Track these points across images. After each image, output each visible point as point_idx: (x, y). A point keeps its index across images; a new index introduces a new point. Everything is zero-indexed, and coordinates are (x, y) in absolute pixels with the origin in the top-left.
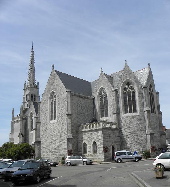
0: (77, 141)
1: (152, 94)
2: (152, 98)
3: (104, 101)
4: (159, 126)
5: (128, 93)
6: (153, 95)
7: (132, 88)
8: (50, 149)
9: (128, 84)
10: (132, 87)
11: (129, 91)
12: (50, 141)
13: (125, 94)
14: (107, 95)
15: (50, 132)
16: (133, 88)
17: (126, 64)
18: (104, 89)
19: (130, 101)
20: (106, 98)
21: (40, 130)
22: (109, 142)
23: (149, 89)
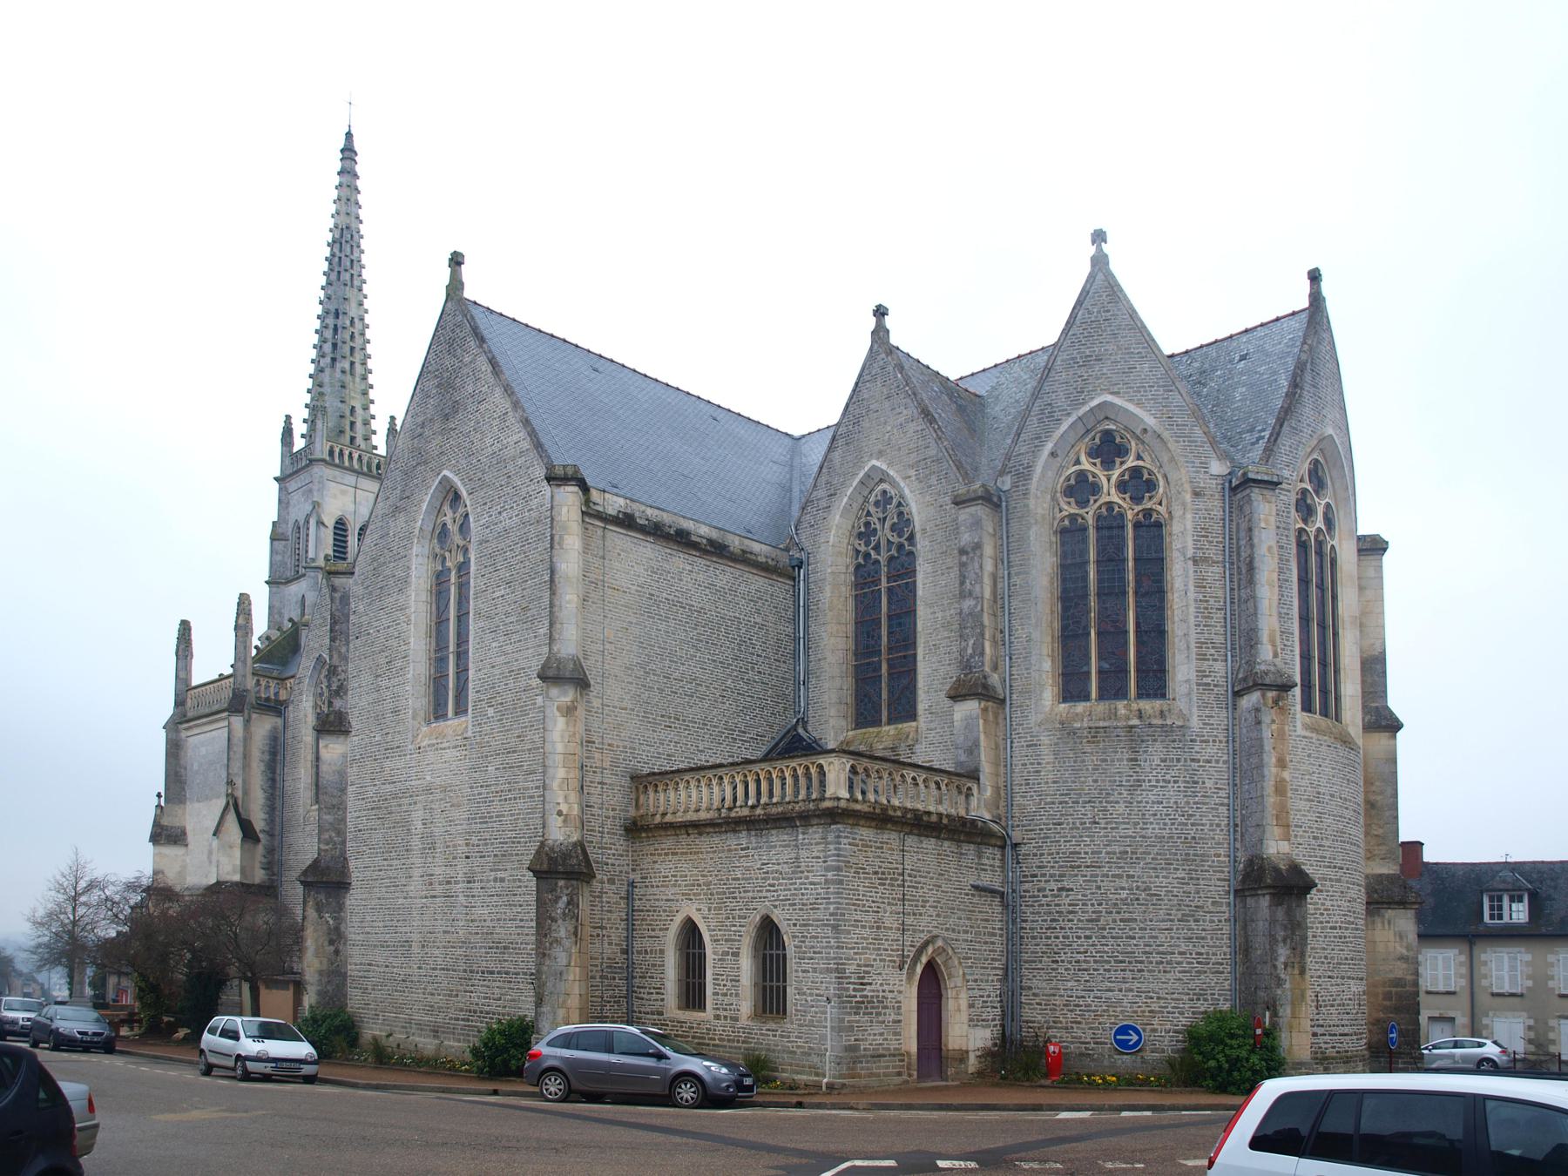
0: (629, 897)
1: (1320, 553)
2: (1321, 587)
3: (889, 589)
4: (1367, 834)
5: (1098, 529)
6: (1333, 562)
7: (1139, 484)
8: (416, 949)
9: (1109, 449)
10: (1136, 472)
11: (1110, 505)
12: (415, 886)
13: (1070, 533)
14: (911, 538)
15: (418, 815)
16: (1151, 486)
17: (1100, 262)
18: (893, 484)
19: (1112, 590)
20: (903, 566)
21: (343, 790)
22: (893, 935)
23: (1293, 498)
